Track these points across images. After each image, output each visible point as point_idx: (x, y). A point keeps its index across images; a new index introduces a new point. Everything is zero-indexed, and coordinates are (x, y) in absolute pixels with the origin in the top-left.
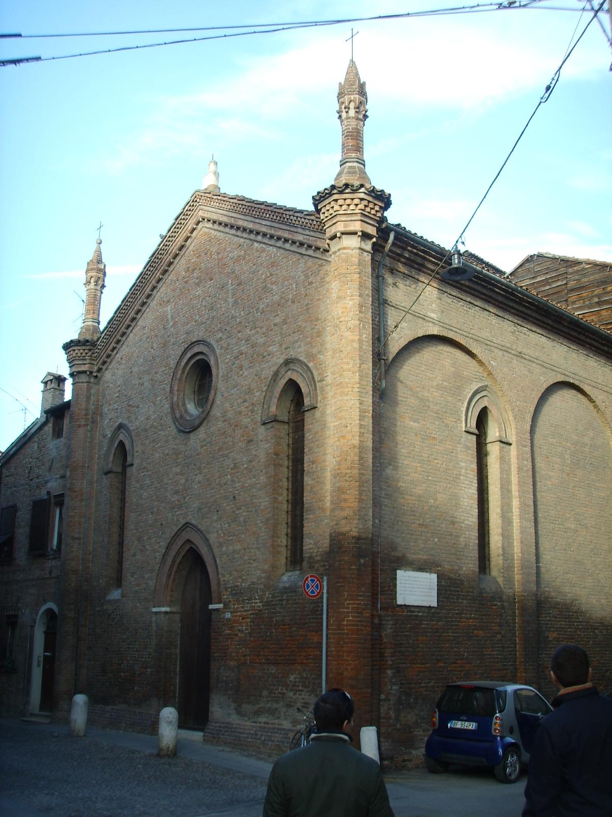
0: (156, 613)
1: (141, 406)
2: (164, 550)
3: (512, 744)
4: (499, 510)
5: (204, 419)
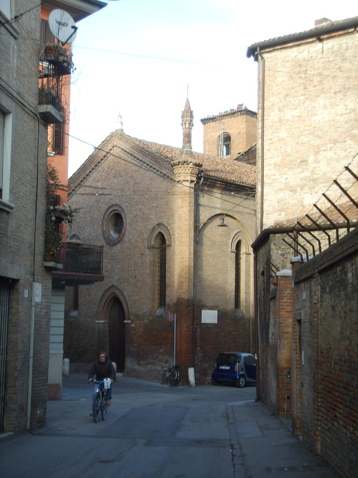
0: (98, 323)
1: (86, 228)
2: (101, 296)
3: (242, 375)
4: (244, 283)
5: (120, 240)
